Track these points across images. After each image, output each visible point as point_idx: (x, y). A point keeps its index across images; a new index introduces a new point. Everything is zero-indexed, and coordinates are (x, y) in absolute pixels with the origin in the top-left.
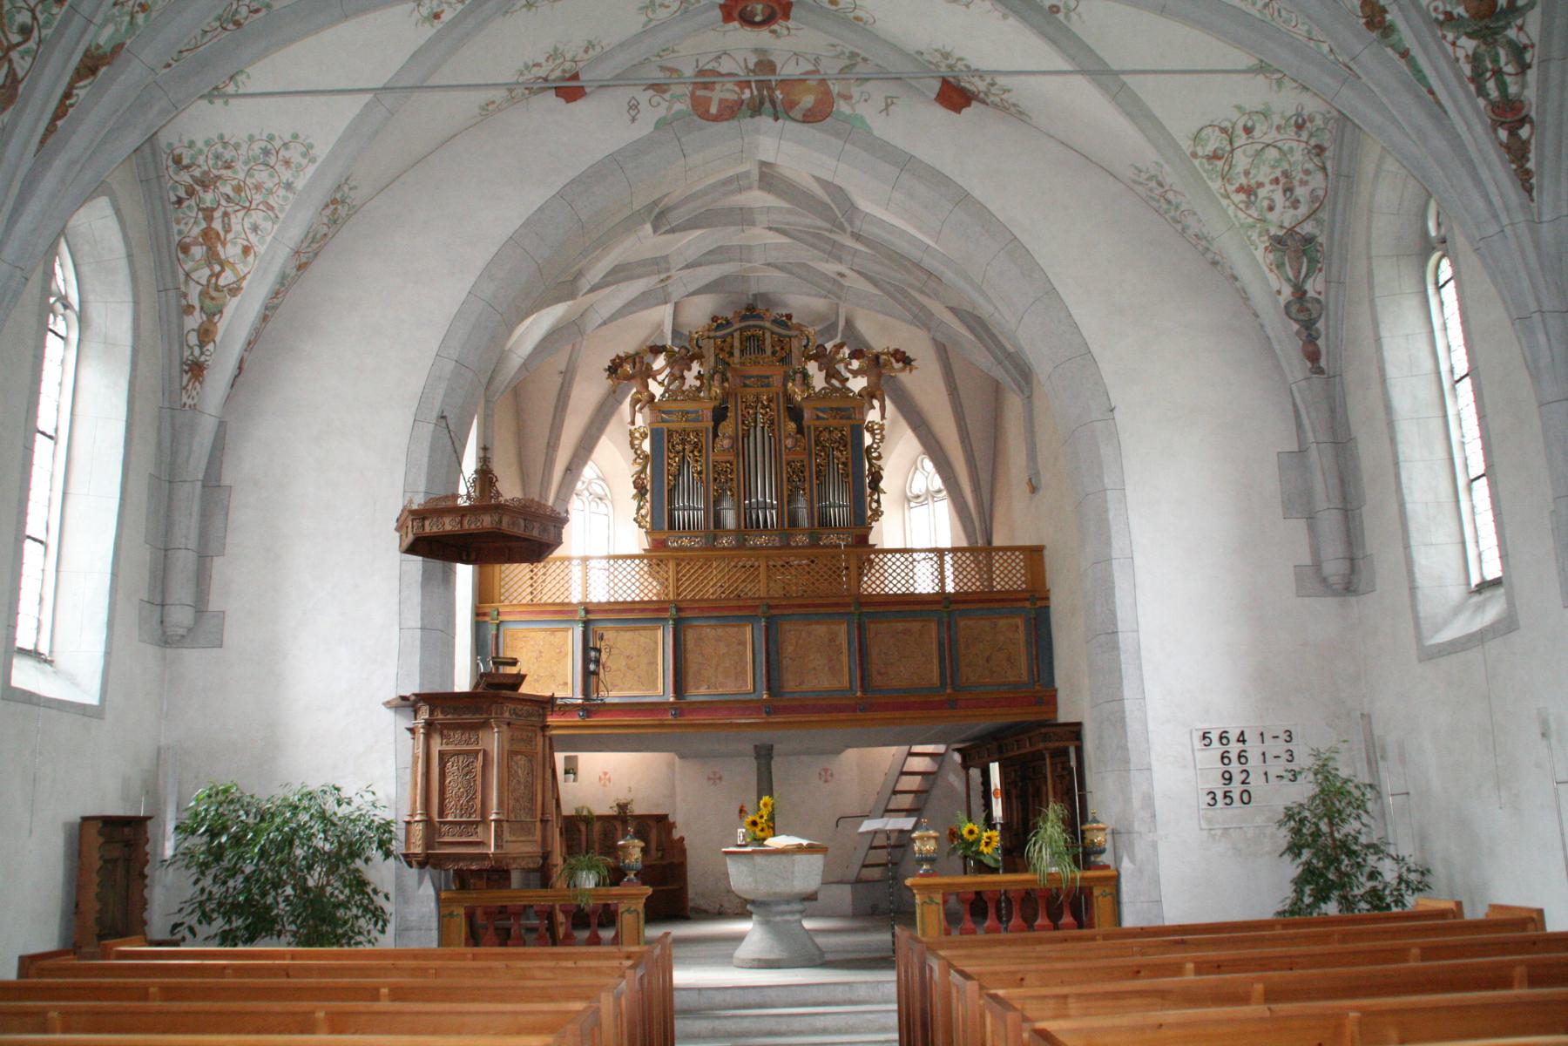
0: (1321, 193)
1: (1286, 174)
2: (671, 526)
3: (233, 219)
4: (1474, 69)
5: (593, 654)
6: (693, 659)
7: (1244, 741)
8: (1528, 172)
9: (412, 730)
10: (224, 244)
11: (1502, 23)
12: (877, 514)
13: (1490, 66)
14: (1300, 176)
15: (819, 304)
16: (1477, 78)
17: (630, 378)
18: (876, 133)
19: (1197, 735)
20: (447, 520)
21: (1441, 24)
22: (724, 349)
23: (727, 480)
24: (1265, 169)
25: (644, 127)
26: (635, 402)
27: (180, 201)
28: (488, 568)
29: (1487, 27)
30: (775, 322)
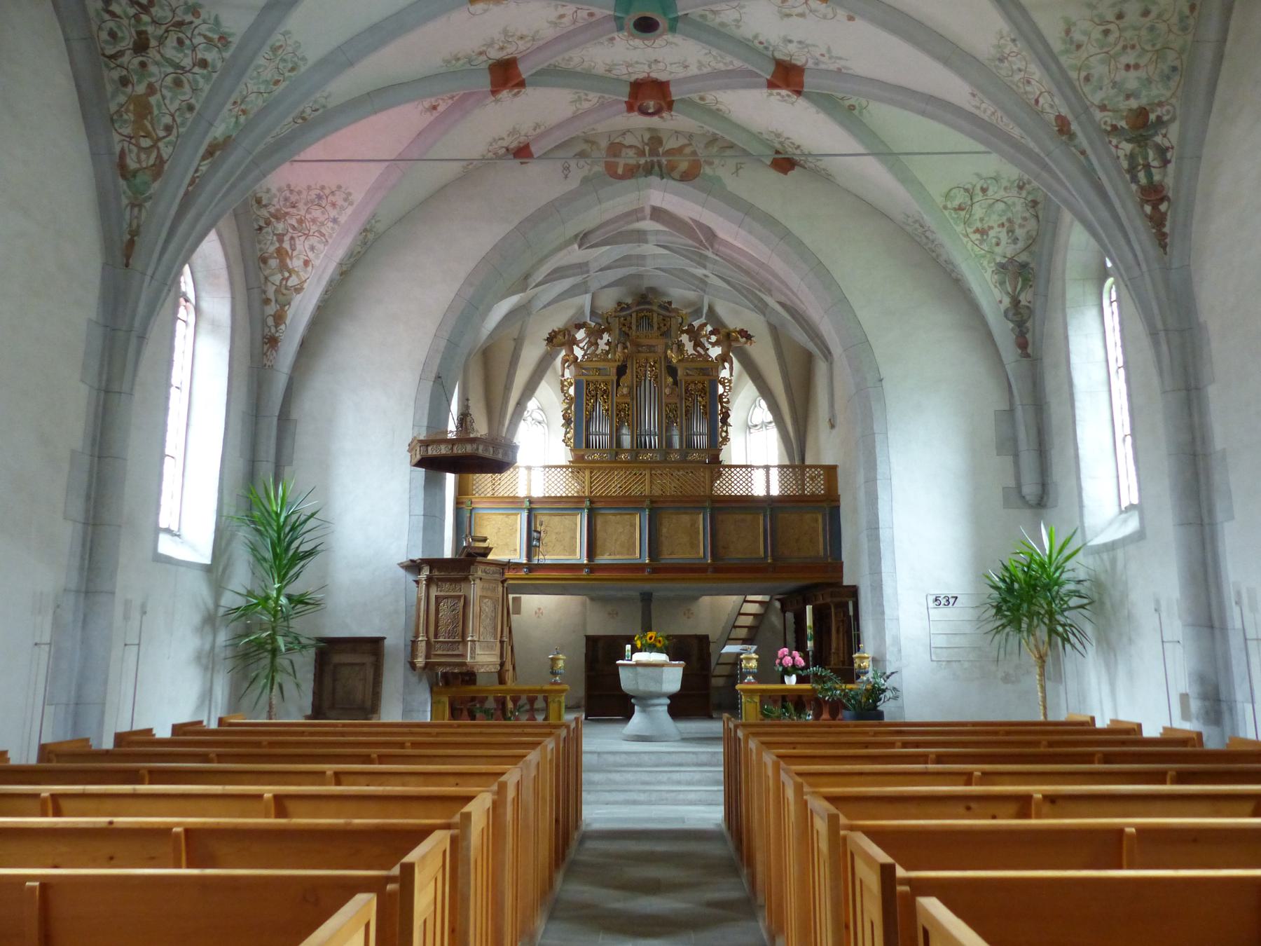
0: (1034, 234)
1: (1009, 220)
2: (588, 446)
3: (297, 242)
4: (1130, 164)
5: (535, 535)
6: (600, 534)
8: (1164, 235)
9: (417, 582)
10: (291, 258)
12: (726, 439)
13: (1141, 161)
14: (1020, 221)
15: (691, 295)
16: (1132, 170)
17: (562, 345)
18: (729, 189)
19: (931, 598)
20: (443, 447)
21: (1108, 133)
22: (626, 324)
23: (624, 415)
24: (995, 217)
25: (573, 184)
26: (564, 361)
27: (260, 229)
28: (465, 475)
30: (660, 306)
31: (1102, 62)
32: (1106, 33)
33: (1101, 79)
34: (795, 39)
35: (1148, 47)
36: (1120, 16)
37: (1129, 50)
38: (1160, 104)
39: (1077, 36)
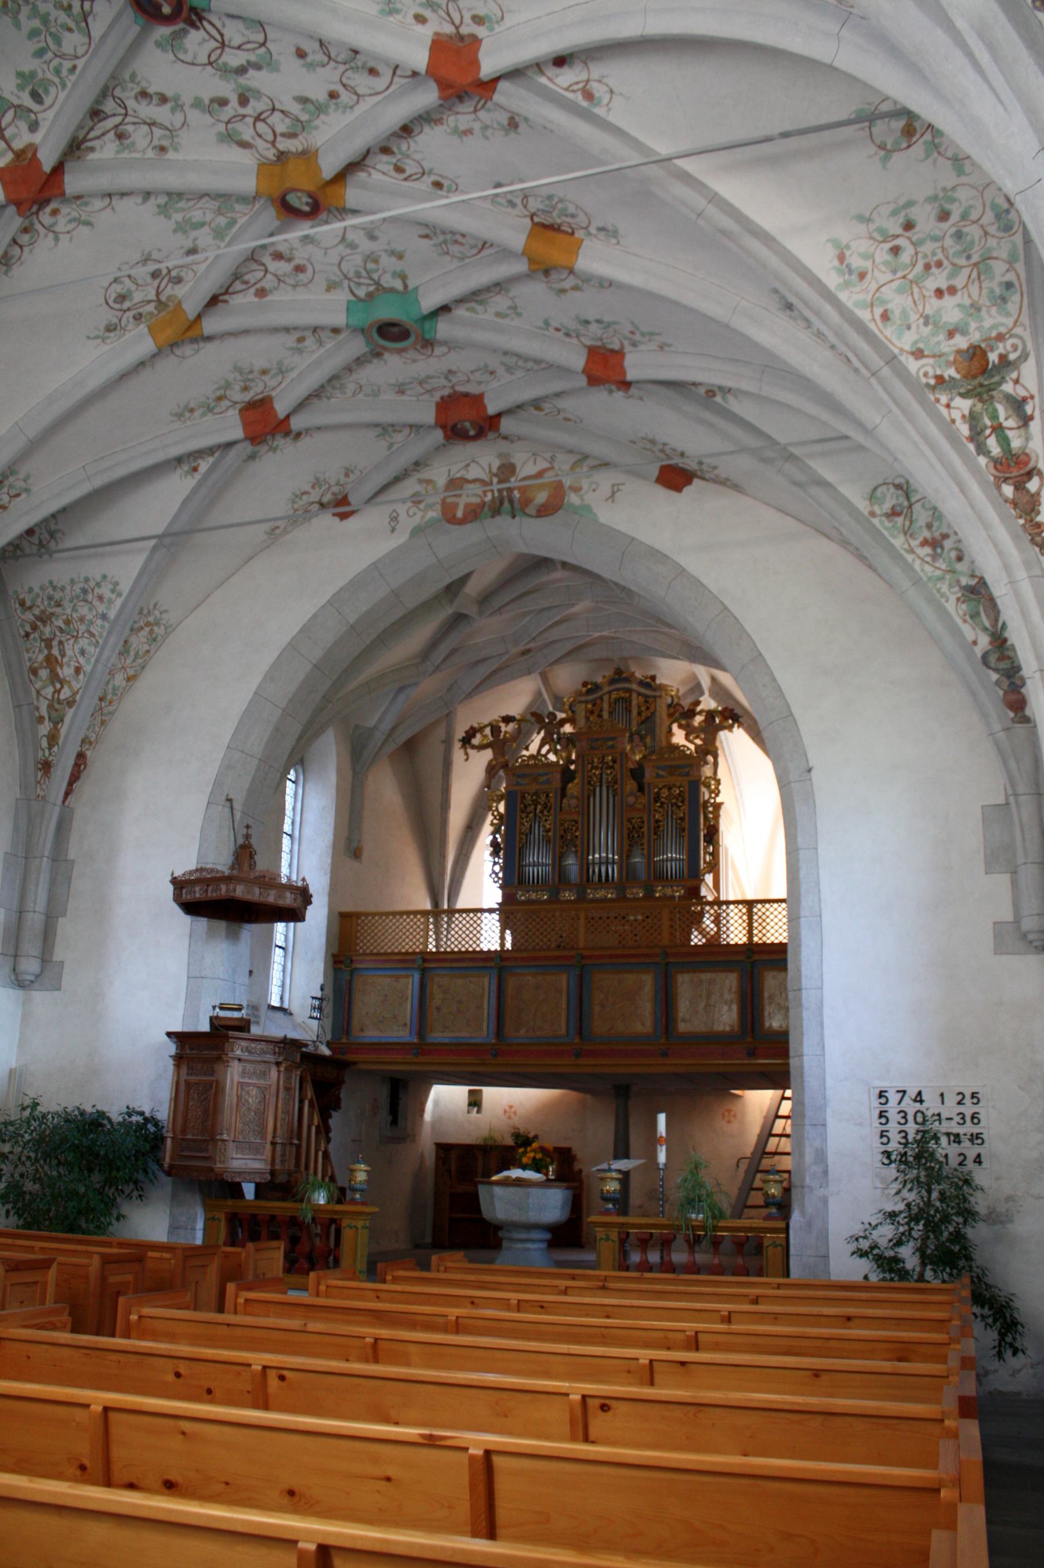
7: (921, 1101)
10: (61, 667)
11: (996, 379)
13: (988, 423)
16: (976, 436)
18: (602, 520)
19: (877, 1091)
21: (933, 388)
27: (27, 635)
29: (981, 385)
31: (900, 291)
32: (896, 251)
33: (904, 313)
34: (591, 319)
35: (962, 262)
36: (909, 226)
37: (934, 270)
38: (1000, 337)
39: (856, 262)
